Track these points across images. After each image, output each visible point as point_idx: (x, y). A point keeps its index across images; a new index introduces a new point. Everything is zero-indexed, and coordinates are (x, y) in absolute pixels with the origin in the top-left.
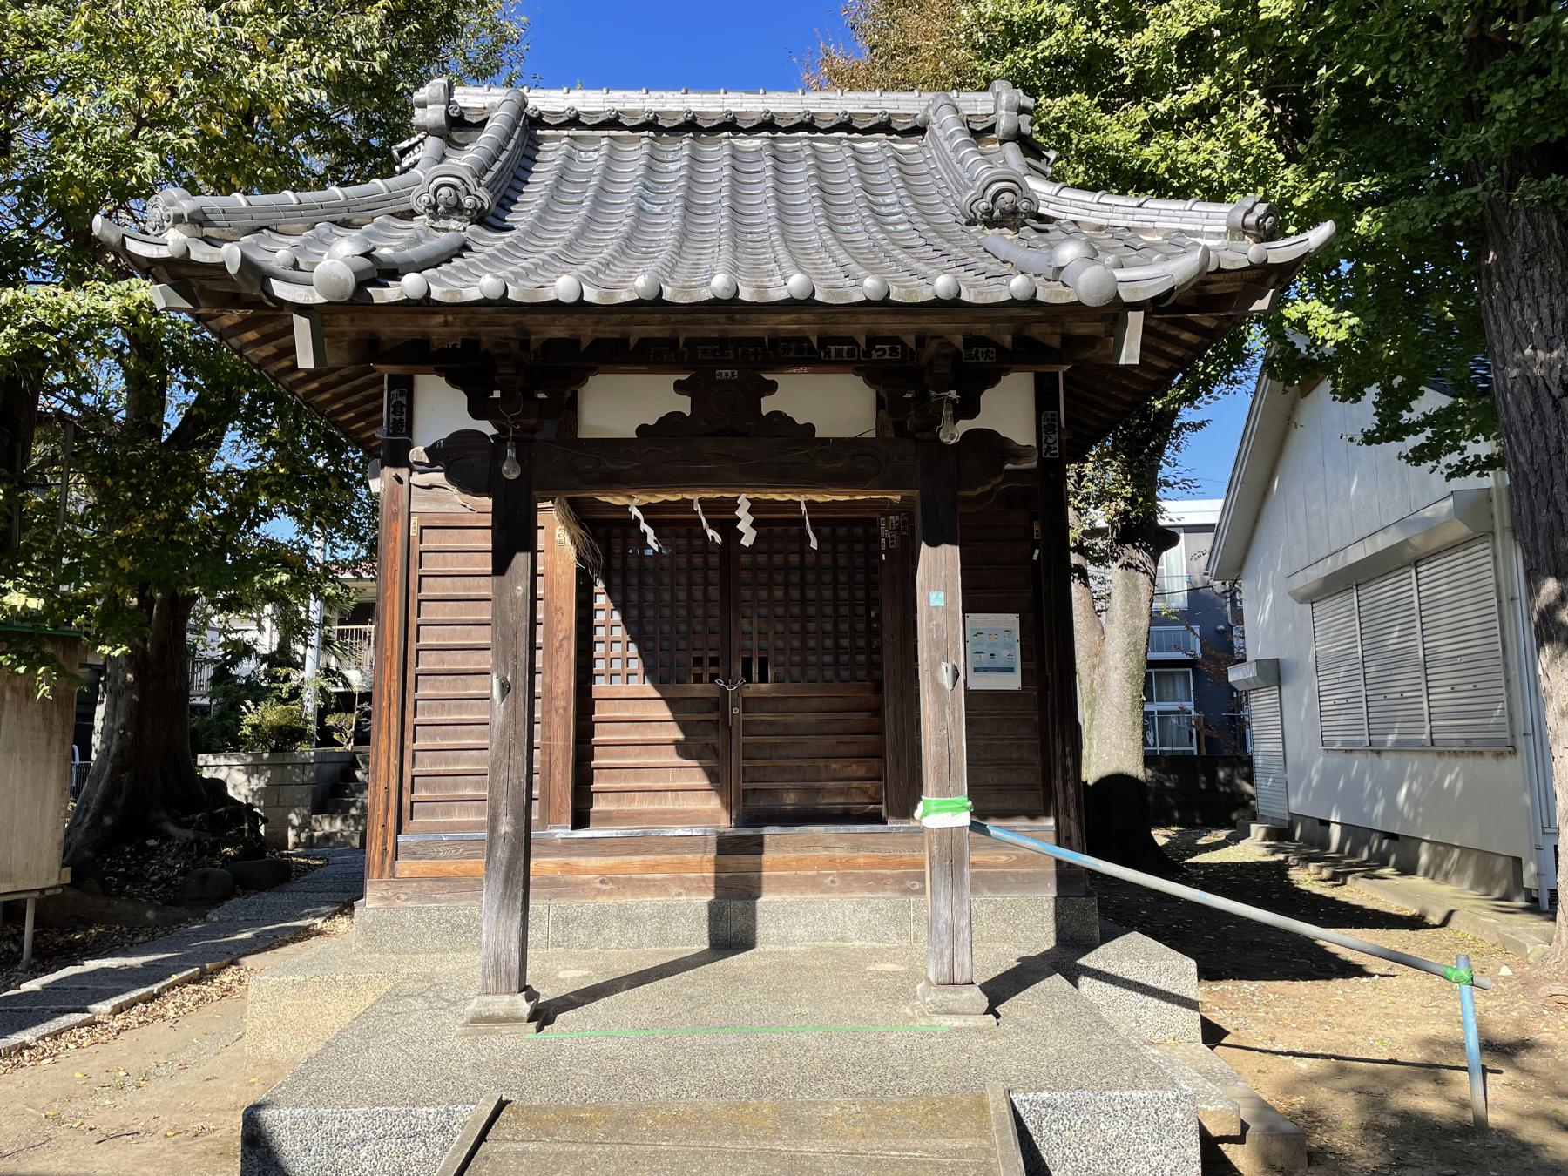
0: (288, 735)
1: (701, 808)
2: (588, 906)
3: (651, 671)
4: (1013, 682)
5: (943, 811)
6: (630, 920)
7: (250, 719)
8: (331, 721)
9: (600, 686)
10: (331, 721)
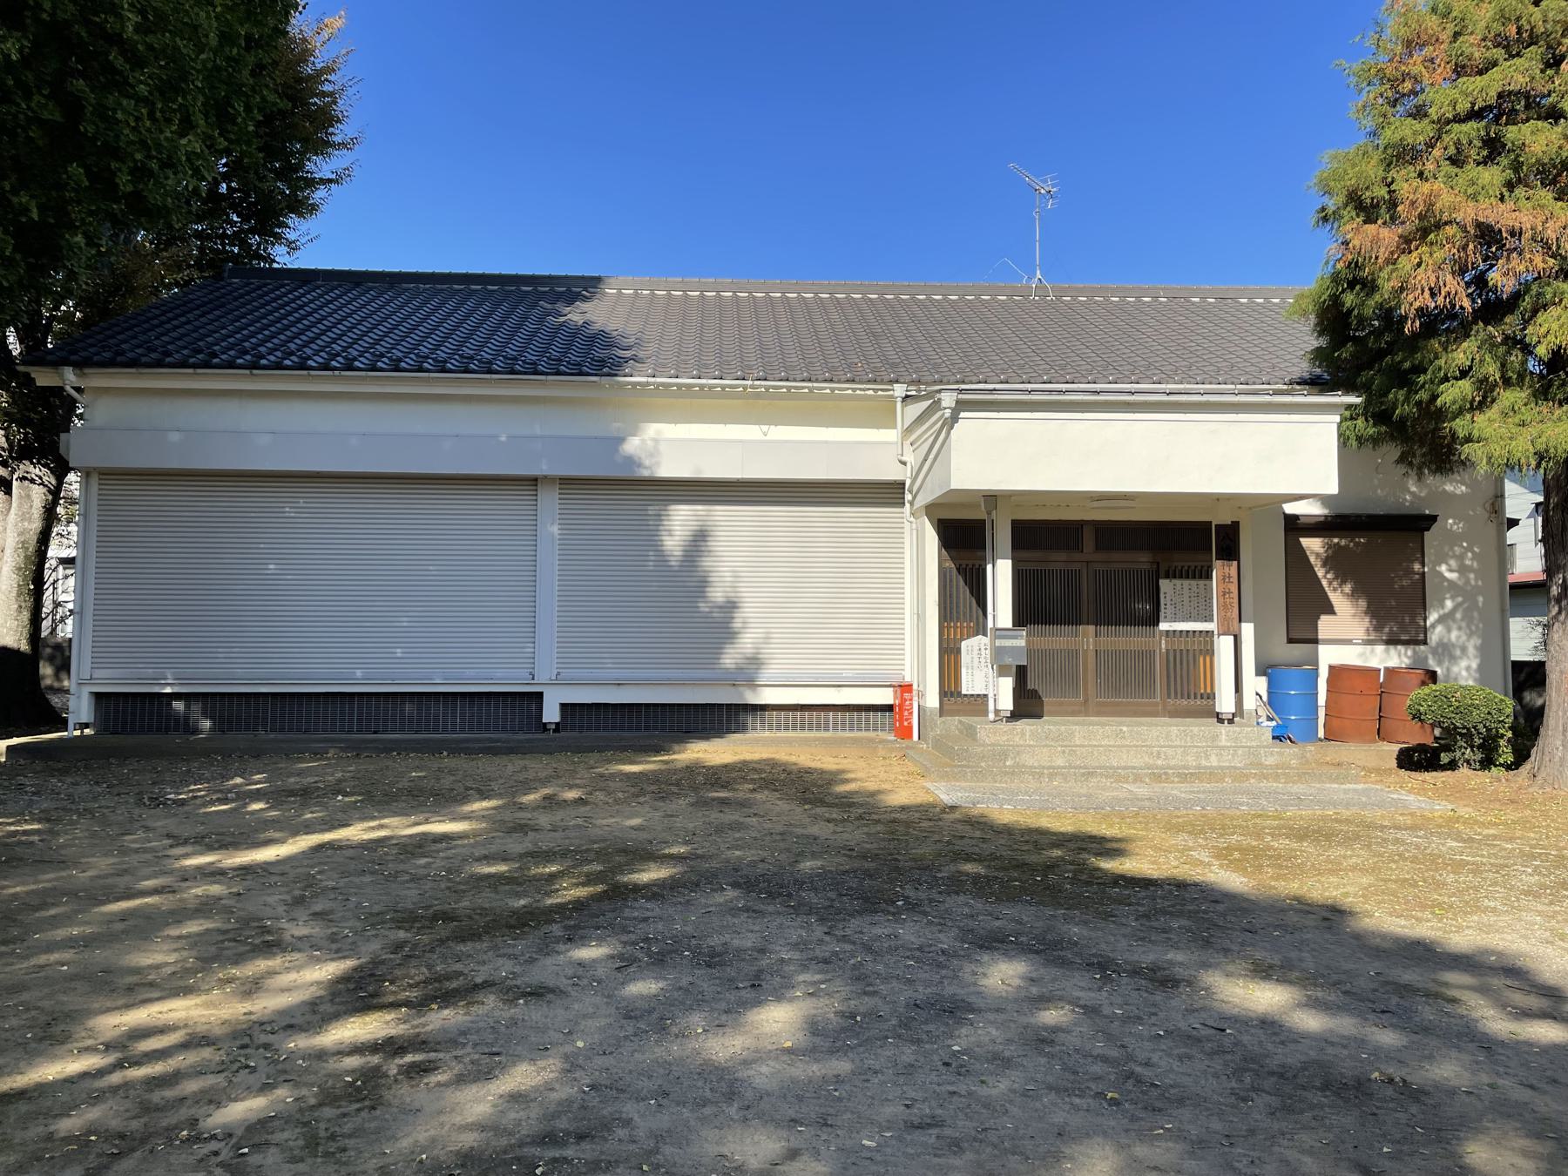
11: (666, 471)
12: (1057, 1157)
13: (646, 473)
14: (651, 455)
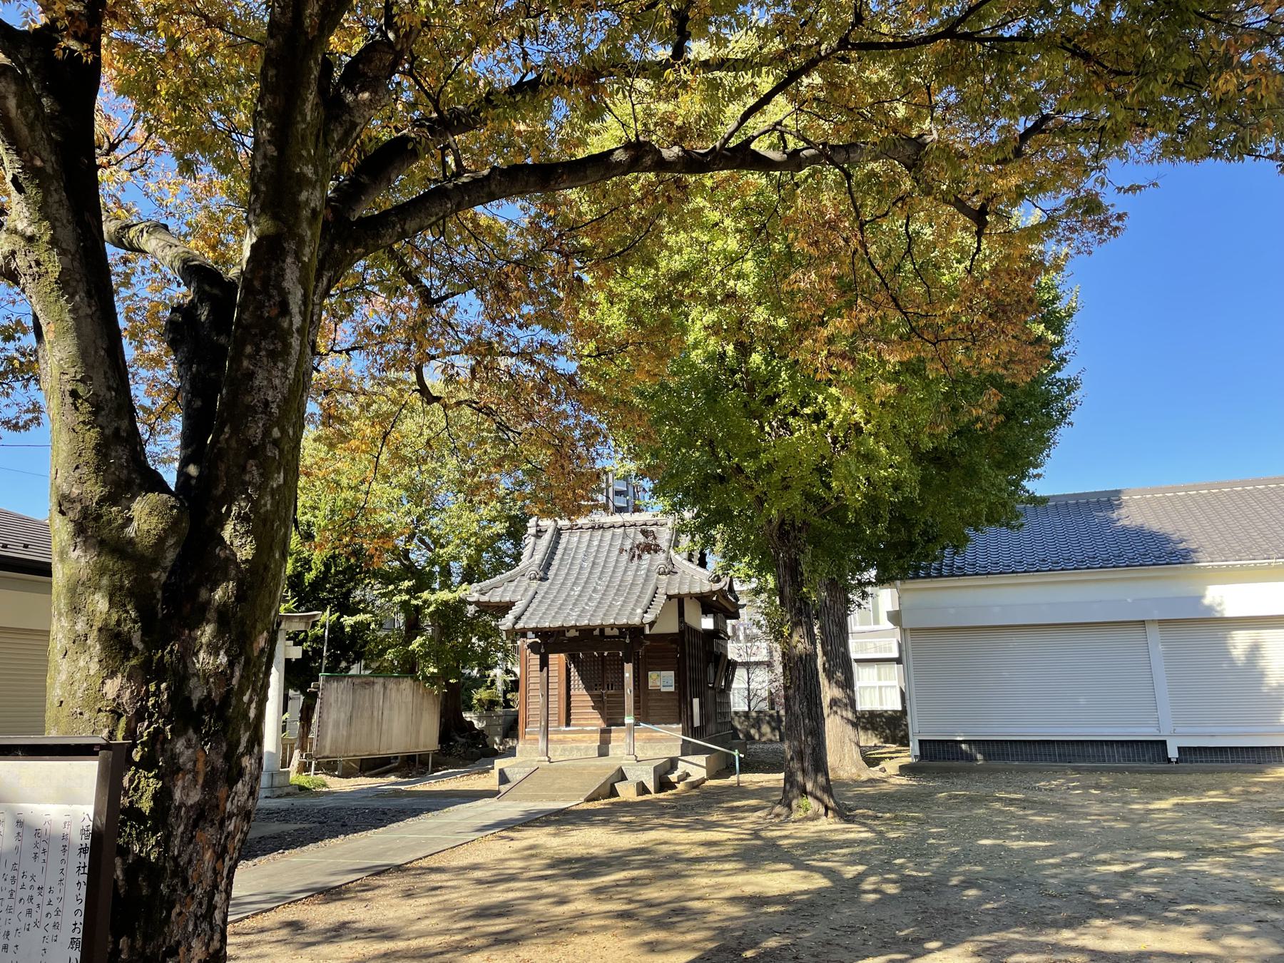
0: (492, 703)
1: (599, 723)
2: (568, 746)
3: (587, 689)
4: (672, 689)
5: (629, 720)
6: (578, 749)
7: (477, 696)
8: (509, 696)
9: (572, 692)
10: (509, 696)
11: (1228, 614)
12: (915, 946)
13: (1218, 615)
14: (1220, 604)
